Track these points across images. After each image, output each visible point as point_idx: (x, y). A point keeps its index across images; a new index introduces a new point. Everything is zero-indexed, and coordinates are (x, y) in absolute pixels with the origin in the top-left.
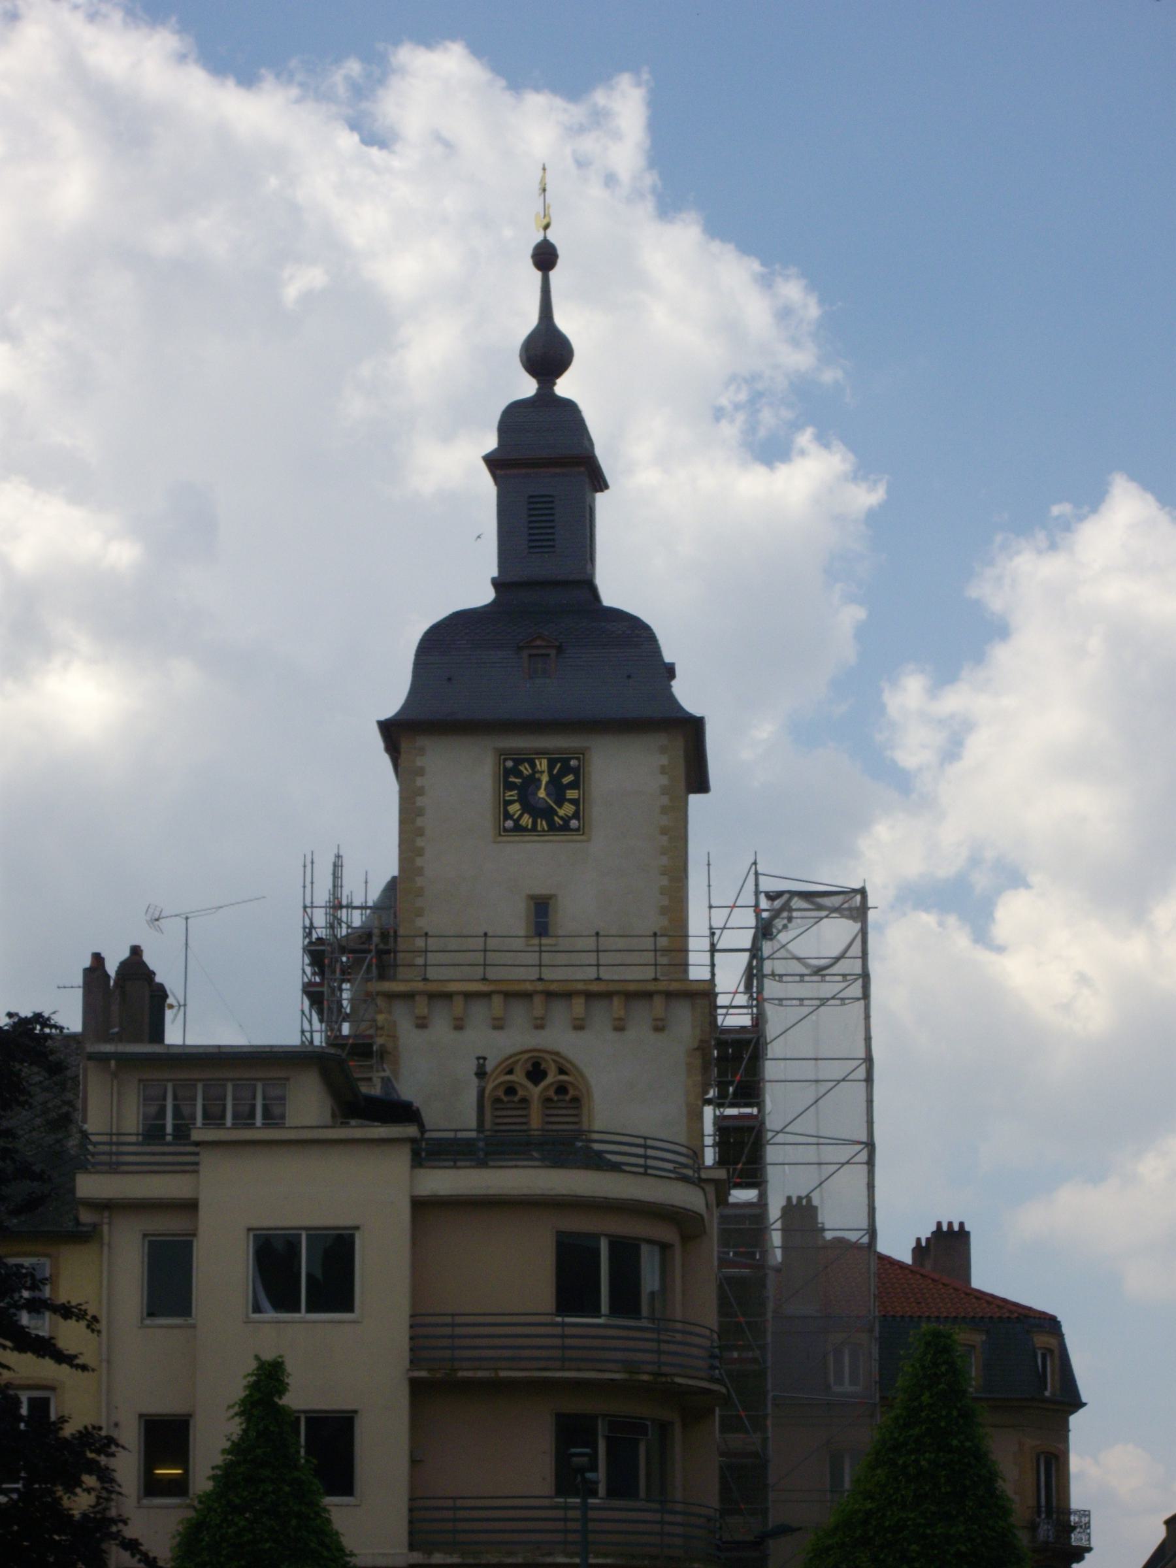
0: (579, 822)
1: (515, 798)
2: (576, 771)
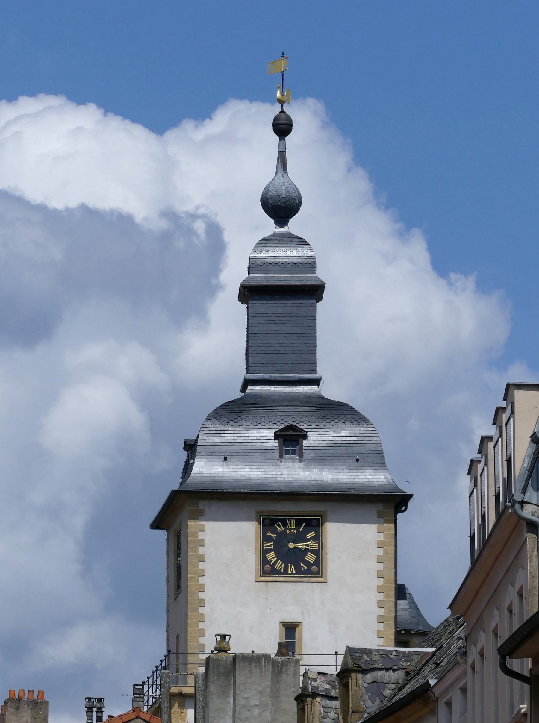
1: (272, 548)
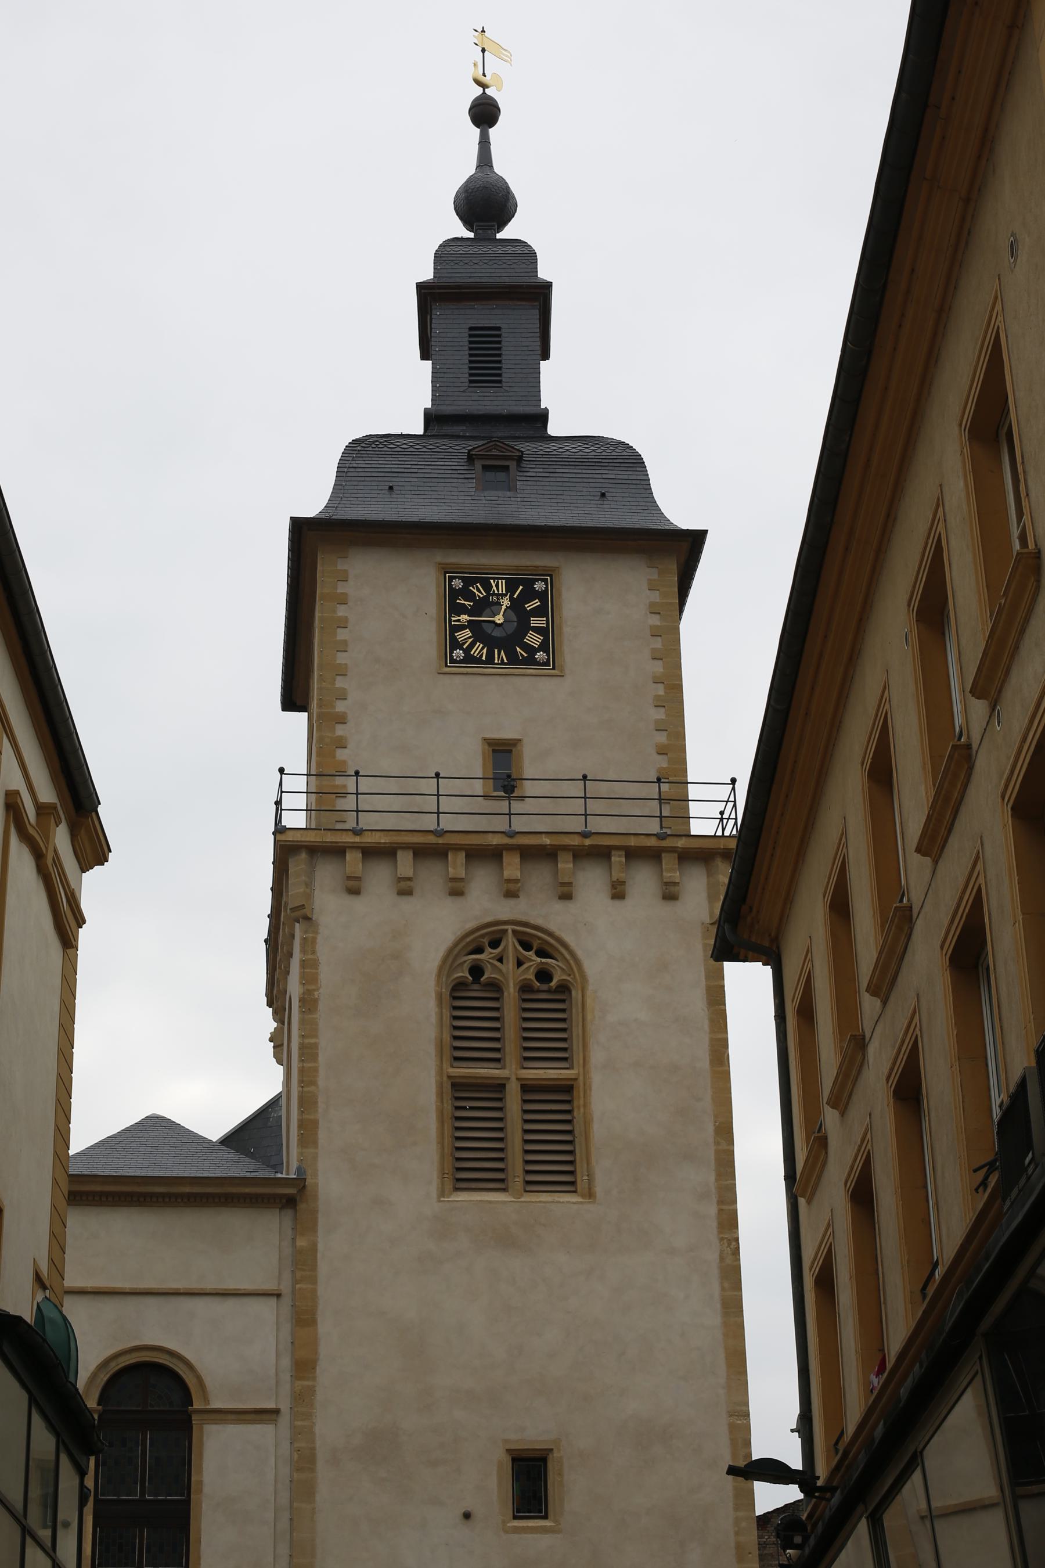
0: (548, 655)
2: (542, 596)
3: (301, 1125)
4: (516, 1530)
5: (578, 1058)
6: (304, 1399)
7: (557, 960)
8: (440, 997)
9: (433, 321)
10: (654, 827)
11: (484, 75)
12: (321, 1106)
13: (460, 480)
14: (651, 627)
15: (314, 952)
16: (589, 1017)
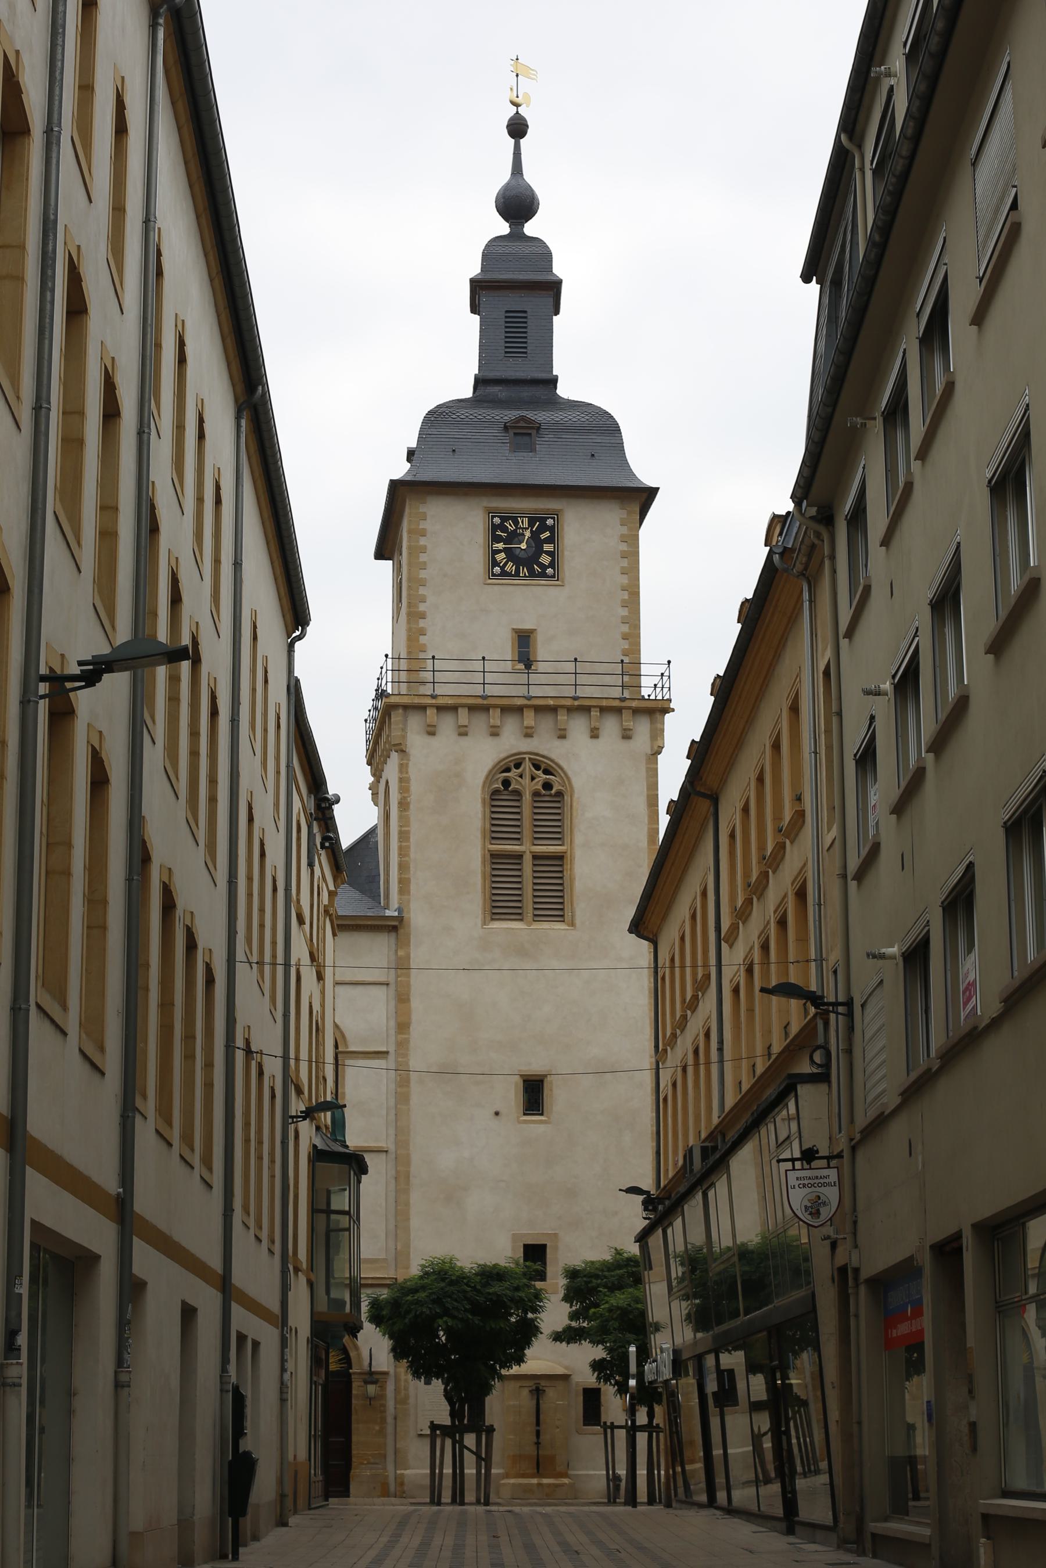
2: (551, 529)
3: (400, 881)
4: (525, 1122)
5: (567, 839)
6: (403, 1046)
7: (555, 776)
8: (484, 801)
9: (481, 306)
10: (617, 693)
11: (517, 97)
12: (412, 869)
13: (499, 445)
14: (621, 551)
15: (407, 773)
16: (574, 814)
